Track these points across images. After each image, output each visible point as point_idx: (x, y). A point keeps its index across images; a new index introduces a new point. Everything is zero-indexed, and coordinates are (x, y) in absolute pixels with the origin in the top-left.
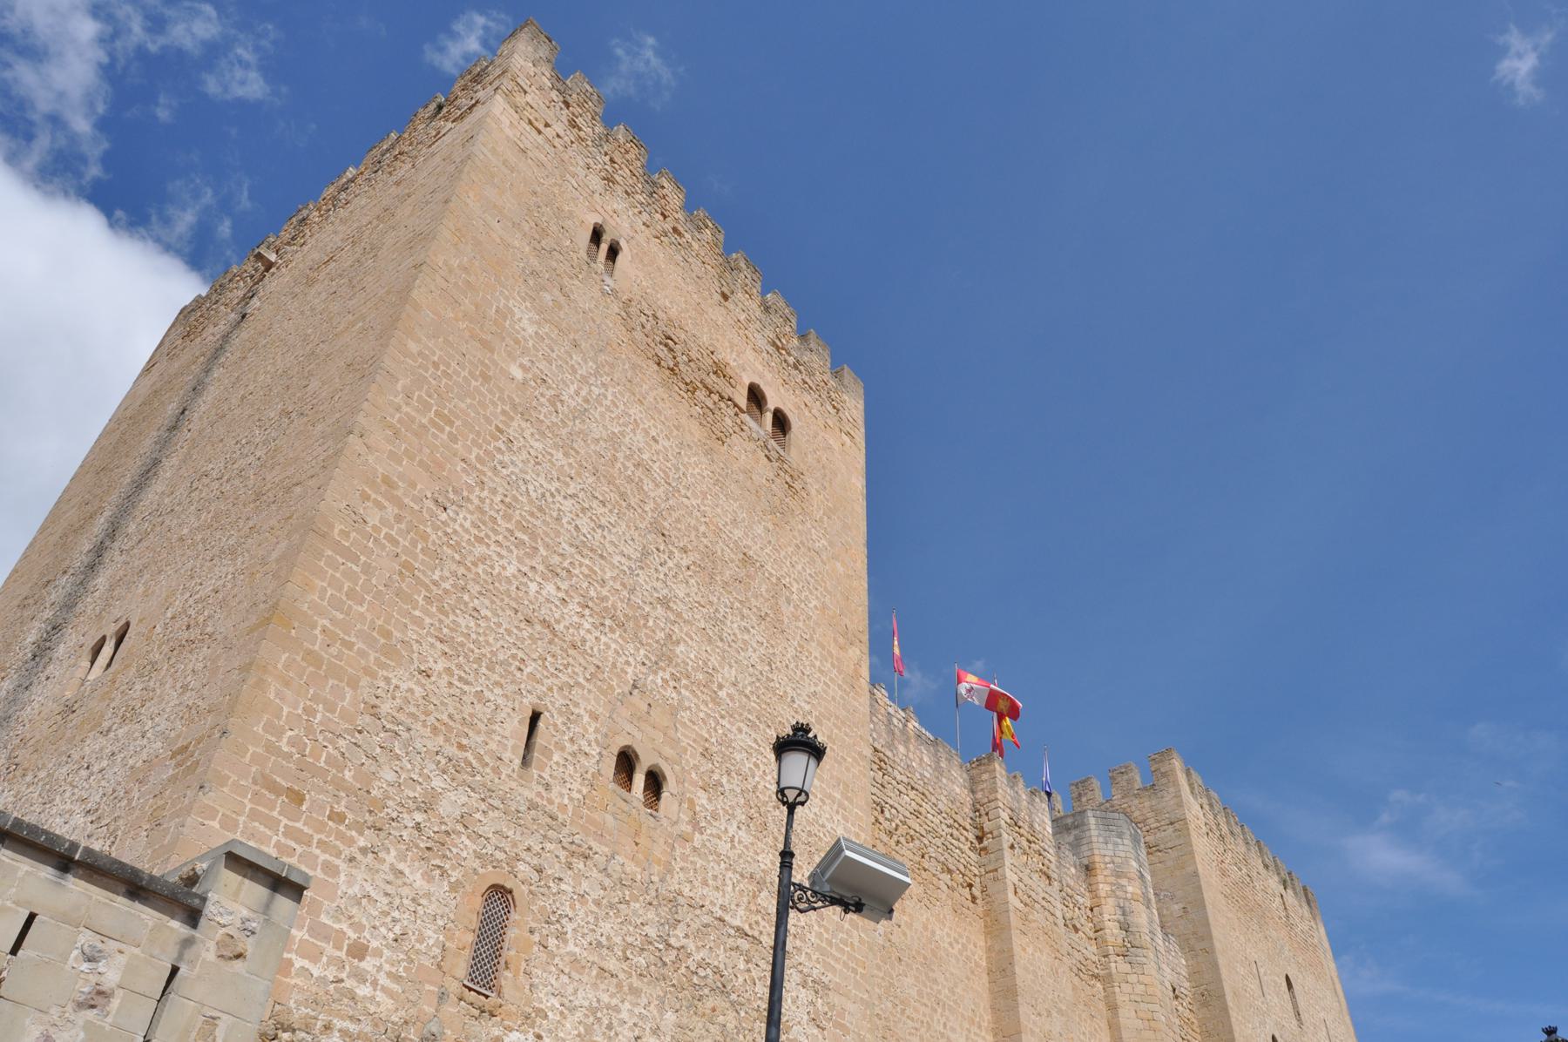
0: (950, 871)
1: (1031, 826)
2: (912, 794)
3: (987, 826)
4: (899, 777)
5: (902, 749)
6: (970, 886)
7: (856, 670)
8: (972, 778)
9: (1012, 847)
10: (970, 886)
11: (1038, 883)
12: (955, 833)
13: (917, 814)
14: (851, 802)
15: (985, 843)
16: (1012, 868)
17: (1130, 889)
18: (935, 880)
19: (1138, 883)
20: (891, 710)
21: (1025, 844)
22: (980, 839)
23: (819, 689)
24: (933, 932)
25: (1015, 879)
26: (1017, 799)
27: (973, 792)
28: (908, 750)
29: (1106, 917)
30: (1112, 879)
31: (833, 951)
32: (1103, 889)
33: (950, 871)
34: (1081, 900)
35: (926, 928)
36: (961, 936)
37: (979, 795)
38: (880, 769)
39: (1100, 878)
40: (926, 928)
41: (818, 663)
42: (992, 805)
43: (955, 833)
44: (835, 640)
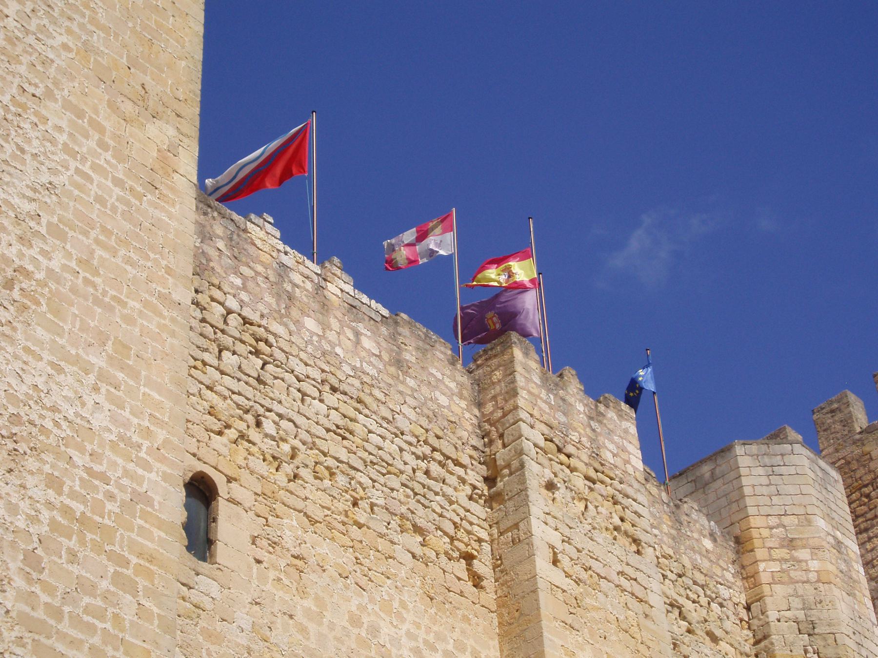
0: (418, 530)
1: (596, 455)
2: (332, 399)
3: (502, 455)
4: (300, 369)
5: (310, 323)
6: (468, 558)
7: (162, 159)
8: (477, 382)
9: (550, 486)
10: (468, 558)
11: (612, 554)
12: (435, 468)
13: (342, 433)
14: (134, 374)
15: (500, 485)
16: (545, 523)
17: (814, 565)
18: (382, 544)
19: (831, 554)
20: (284, 259)
21: (580, 483)
22: (490, 481)
23: (61, 179)
24: (374, 631)
25: (555, 538)
26: (565, 406)
27: (480, 405)
28: (325, 327)
29: (772, 615)
30: (783, 553)
31: (65, 627)
32: (766, 569)
33: (418, 530)
34: (725, 593)
35: (355, 621)
36: (439, 637)
37: (489, 407)
38: (257, 353)
39: (760, 553)
40: (355, 621)
41: (62, 138)
42: (510, 418)
43: (435, 468)
44: (111, 105)
